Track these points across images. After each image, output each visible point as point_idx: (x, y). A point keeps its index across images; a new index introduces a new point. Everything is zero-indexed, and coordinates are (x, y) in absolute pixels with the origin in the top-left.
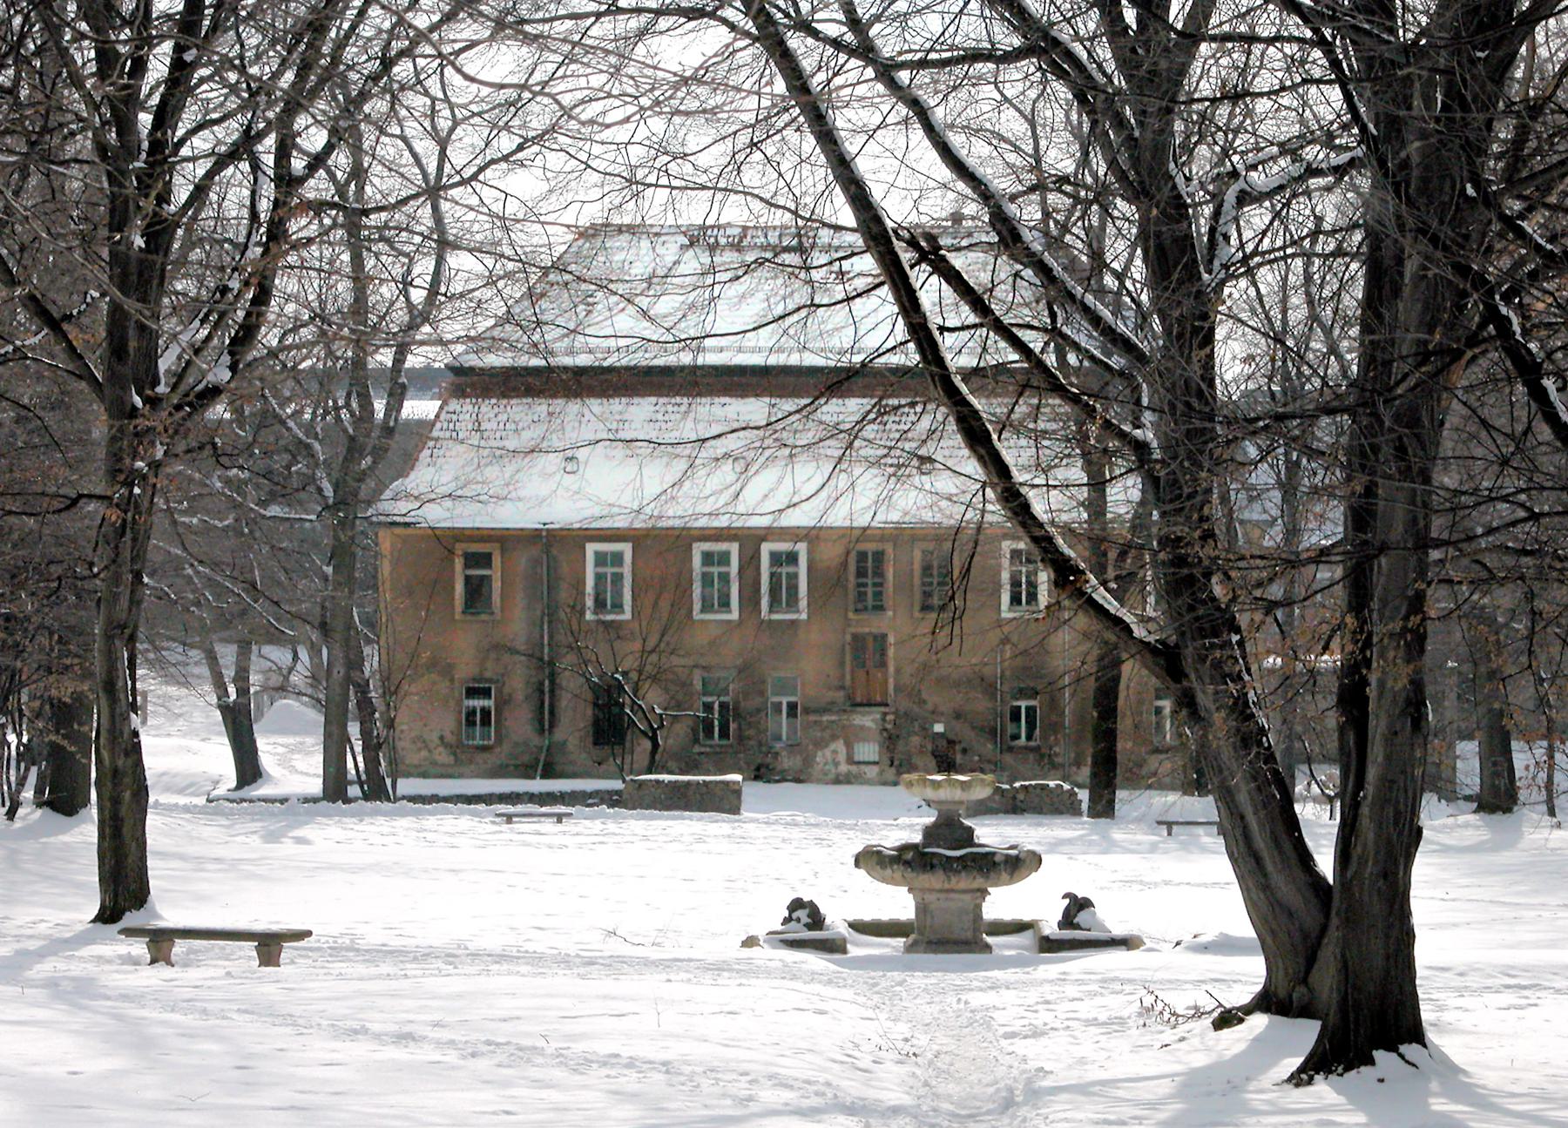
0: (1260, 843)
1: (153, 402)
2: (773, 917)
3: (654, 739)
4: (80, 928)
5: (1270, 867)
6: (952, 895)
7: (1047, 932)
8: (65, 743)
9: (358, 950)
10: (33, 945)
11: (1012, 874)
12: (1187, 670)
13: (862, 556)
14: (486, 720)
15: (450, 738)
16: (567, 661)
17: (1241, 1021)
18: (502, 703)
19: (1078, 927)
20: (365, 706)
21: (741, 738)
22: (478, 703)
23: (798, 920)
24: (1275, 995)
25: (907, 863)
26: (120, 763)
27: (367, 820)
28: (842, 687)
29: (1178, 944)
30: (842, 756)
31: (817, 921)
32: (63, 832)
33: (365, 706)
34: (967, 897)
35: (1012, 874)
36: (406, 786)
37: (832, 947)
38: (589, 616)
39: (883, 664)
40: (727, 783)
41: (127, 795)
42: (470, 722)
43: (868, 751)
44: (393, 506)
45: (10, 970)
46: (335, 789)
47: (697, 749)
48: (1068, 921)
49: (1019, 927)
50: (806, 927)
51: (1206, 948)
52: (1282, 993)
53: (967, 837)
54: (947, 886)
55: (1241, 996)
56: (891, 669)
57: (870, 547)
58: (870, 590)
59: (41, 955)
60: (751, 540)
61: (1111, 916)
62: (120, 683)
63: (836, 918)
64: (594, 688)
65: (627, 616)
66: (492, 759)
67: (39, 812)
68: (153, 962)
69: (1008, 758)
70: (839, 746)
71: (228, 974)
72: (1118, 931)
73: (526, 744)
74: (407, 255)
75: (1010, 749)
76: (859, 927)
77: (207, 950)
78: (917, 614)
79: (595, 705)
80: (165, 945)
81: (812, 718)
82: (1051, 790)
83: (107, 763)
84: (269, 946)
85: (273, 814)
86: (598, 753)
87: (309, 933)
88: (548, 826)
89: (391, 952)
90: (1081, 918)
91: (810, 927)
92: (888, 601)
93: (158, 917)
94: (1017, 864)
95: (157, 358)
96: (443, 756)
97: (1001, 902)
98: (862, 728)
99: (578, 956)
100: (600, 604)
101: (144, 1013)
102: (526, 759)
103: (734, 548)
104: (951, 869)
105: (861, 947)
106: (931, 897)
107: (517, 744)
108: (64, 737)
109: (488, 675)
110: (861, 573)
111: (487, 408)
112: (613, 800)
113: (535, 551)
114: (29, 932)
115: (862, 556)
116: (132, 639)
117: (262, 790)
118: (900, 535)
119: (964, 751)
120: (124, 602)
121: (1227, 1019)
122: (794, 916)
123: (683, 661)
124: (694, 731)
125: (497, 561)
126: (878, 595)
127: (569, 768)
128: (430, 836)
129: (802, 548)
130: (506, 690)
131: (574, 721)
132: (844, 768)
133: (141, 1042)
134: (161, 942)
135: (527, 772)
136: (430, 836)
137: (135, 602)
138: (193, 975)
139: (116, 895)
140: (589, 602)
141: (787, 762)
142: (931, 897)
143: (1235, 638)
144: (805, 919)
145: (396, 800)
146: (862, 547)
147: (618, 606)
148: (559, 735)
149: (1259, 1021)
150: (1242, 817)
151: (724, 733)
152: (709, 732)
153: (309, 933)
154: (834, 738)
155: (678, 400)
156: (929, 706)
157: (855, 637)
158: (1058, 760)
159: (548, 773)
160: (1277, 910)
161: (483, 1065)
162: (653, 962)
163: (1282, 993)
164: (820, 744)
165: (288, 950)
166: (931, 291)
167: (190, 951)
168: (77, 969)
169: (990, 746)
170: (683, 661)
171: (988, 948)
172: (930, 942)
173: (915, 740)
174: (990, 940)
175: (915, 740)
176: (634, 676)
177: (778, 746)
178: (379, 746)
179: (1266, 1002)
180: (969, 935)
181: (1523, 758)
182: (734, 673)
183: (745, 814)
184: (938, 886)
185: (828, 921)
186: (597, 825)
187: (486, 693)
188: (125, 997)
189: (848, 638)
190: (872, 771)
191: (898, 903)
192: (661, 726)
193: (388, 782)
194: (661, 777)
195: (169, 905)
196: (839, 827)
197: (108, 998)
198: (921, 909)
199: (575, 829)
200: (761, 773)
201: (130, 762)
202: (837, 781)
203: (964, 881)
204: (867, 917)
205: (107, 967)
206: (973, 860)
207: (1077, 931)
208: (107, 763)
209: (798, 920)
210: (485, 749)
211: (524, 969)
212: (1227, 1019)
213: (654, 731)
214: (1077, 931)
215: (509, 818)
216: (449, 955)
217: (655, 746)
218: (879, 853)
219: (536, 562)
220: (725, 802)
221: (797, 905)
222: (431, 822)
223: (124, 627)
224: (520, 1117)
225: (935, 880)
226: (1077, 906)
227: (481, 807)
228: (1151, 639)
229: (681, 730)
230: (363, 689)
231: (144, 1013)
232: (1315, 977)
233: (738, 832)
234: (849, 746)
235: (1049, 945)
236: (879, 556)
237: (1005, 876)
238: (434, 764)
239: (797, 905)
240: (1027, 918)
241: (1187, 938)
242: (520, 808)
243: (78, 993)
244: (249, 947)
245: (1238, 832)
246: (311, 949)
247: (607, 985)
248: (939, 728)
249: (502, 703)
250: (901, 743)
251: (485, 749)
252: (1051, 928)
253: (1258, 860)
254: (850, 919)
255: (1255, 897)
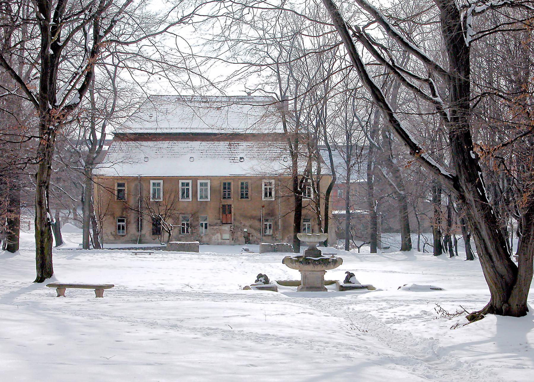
0: (491, 250)
1: (55, 107)
2: (252, 280)
3: (169, 233)
4: (30, 284)
5: (495, 259)
6: (315, 272)
7: (341, 284)
8: (12, 232)
9: (127, 291)
10: (16, 290)
11: (334, 265)
12: (462, 185)
13: (225, 184)
14: (123, 228)
15: (113, 233)
16: (145, 212)
17: (483, 317)
18: (127, 224)
19: (350, 282)
20: (94, 223)
21: (192, 233)
22: (121, 223)
23: (261, 281)
24: (495, 307)
25: (301, 262)
26: (44, 229)
27: (96, 254)
28: (219, 219)
29: (400, 288)
30: (220, 238)
31: (267, 281)
32: (11, 257)
33: (94, 223)
34: (319, 273)
35: (334, 265)
36: (105, 246)
37: (274, 289)
38: (151, 200)
39: (230, 213)
40: (195, 244)
41: (46, 239)
42: (119, 229)
43: (227, 236)
44: (95, 171)
45: (8, 299)
46: (86, 246)
47: (180, 236)
48: (347, 280)
49: (331, 283)
50: (263, 282)
51: (409, 289)
52: (498, 306)
53: (319, 254)
54: (313, 269)
55: (480, 306)
56: (233, 214)
57: (227, 181)
58: (227, 193)
59: (19, 293)
60: (195, 179)
61: (361, 279)
62: (44, 202)
63: (273, 279)
64: (153, 219)
65: (162, 200)
66: (125, 239)
67: (4, 251)
68: (58, 296)
69: (264, 238)
70: (219, 235)
71: (88, 300)
72: (363, 283)
73: (134, 235)
74: (105, 98)
75: (265, 236)
76: (279, 283)
77: (76, 292)
78: (240, 199)
79: (153, 224)
80: (63, 290)
81: (211, 227)
82: (285, 246)
83: (39, 229)
84: (99, 290)
85: (69, 253)
86: (153, 237)
87: (113, 286)
88: (147, 256)
89: (139, 292)
90: (351, 279)
91: (265, 283)
92: (232, 196)
93: (56, 280)
94: (336, 263)
95: (55, 94)
96: (112, 238)
97: (330, 275)
98: (225, 230)
99: (203, 293)
100: (154, 197)
101: (66, 316)
102: (134, 238)
103: (190, 182)
104: (315, 264)
105: (282, 290)
106: (307, 273)
107: (132, 235)
108: (12, 230)
109: (124, 216)
110: (225, 188)
111: (123, 144)
112: (164, 249)
113: (137, 182)
114: (13, 286)
115: (225, 184)
116: (47, 187)
117: (62, 247)
118: (235, 178)
119: (252, 236)
120: (45, 175)
121: (473, 317)
122: (259, 279)
123: (177, 212)
124: (180, 230)
125: (126, 185)
126: (229, 194)
127: (146, 241)
128: (115, 258)
129: (209, 181)
130: (129, 220)
131: (147, 228)
132: (220, 241)
133: (62, 328)
134: (61, 288)
135: (135, 242)
136: (115, 258)
137: (49, 175)
138: (76, 300)
139: (42, 274)
140: (151, 196)
141: (205, 239)
142: (307, 273)
143: (480, 173)
144: (263, 281)
145: (103, 249)
146: (225, 181)
147: (159, 197)
148: (143, 232)
149: (491, 318)
150: (484, 240)
151: (187, 232)
152: (184, 231)
153: (113, 286)
154: (217, 232)
155: (175, 142)
156: (243, 224)
157: (223, 206)
158: (278, 238)
159: (140, 242)
160: (497, 275)
161: (214, 339)
162: (229, 295)
163: (498, 306)
164: (213, 234)
165: (106, 292)
166: (359, 47)
167: (70, 292)
168: (33, 299)
169: (259, 235)
170: (177, 212)
171: (326, 289)
172: (307, 288)
173: (239, 233)
174: (326, 287)
175: (239, 233)
176: (164, 216)
177: (202, 235)
178: (98, 234)
179: (491, 309)
180: (320, 285)
181: (414, 237)
182: (191, 215)
183: (200, 252)
184: (310, 269)
185: (270, 281)
186: (160, 256)
187: (123, 221)
188: (55, 309)
189: (221, 206)
190: (227, 241)
191: (296, 275)
192: (172, 229)
193: (101, 245)
194: (177, 242)
195: (60, 275)
196: (228, 255)
197: (49, 310)
198: (304, 277)
199: (155, 256)
200: (202, 243)
201: (47, 228)
202: (218, 244)
203: (319, 268)
204: (283, 279)
205: (42, 297)
206: (322, 261)
207: (350, 285)
208: (39, 229)
209: (261, 281)
210: (123, 236)
211: (172, 298)
212: (473, 317)
213: (170, 231)
214: (350, 285)
215: (136, 254)
216: (159, 293)
217: (170, 234)
218: (291, 259)
219: (136, 186)
220: (194, 249)
221: (260, 276)
222: (114, 255)
223: (45, 183)
224: (259, 368)
225: (310, 267)
226: (350, 275)
227: (127, 250)
228: (447, 174)
229: (176, 230)
230: (93, 218)
231: (66, 316)
232: (511, 300)
233: (201, 257)
234: (221, 234)
235: (342, 289)
236: (229, 184)
237: (332, 266)
238: (109, 240)
239: (260, 276)
240: (333, 280)
241: (402, 286)
242: (138, 251)
243: (33, 307)
244: (93, 291)
245: (482, 246)
246: (113, 291)
247: (223, 304)
248: (245, 230)
249: (127, 224)
250: (235, 234)
251: (123, 236)
252: (342, 283)
253: (490, 257)
254: (277, 280)
255: (489, 270)
